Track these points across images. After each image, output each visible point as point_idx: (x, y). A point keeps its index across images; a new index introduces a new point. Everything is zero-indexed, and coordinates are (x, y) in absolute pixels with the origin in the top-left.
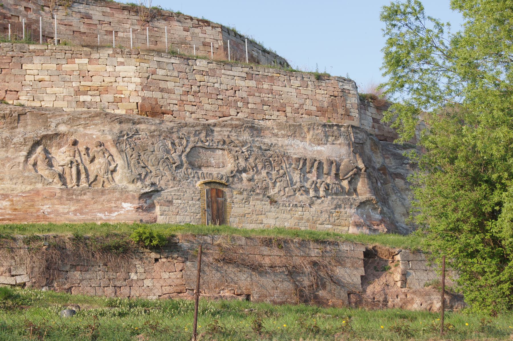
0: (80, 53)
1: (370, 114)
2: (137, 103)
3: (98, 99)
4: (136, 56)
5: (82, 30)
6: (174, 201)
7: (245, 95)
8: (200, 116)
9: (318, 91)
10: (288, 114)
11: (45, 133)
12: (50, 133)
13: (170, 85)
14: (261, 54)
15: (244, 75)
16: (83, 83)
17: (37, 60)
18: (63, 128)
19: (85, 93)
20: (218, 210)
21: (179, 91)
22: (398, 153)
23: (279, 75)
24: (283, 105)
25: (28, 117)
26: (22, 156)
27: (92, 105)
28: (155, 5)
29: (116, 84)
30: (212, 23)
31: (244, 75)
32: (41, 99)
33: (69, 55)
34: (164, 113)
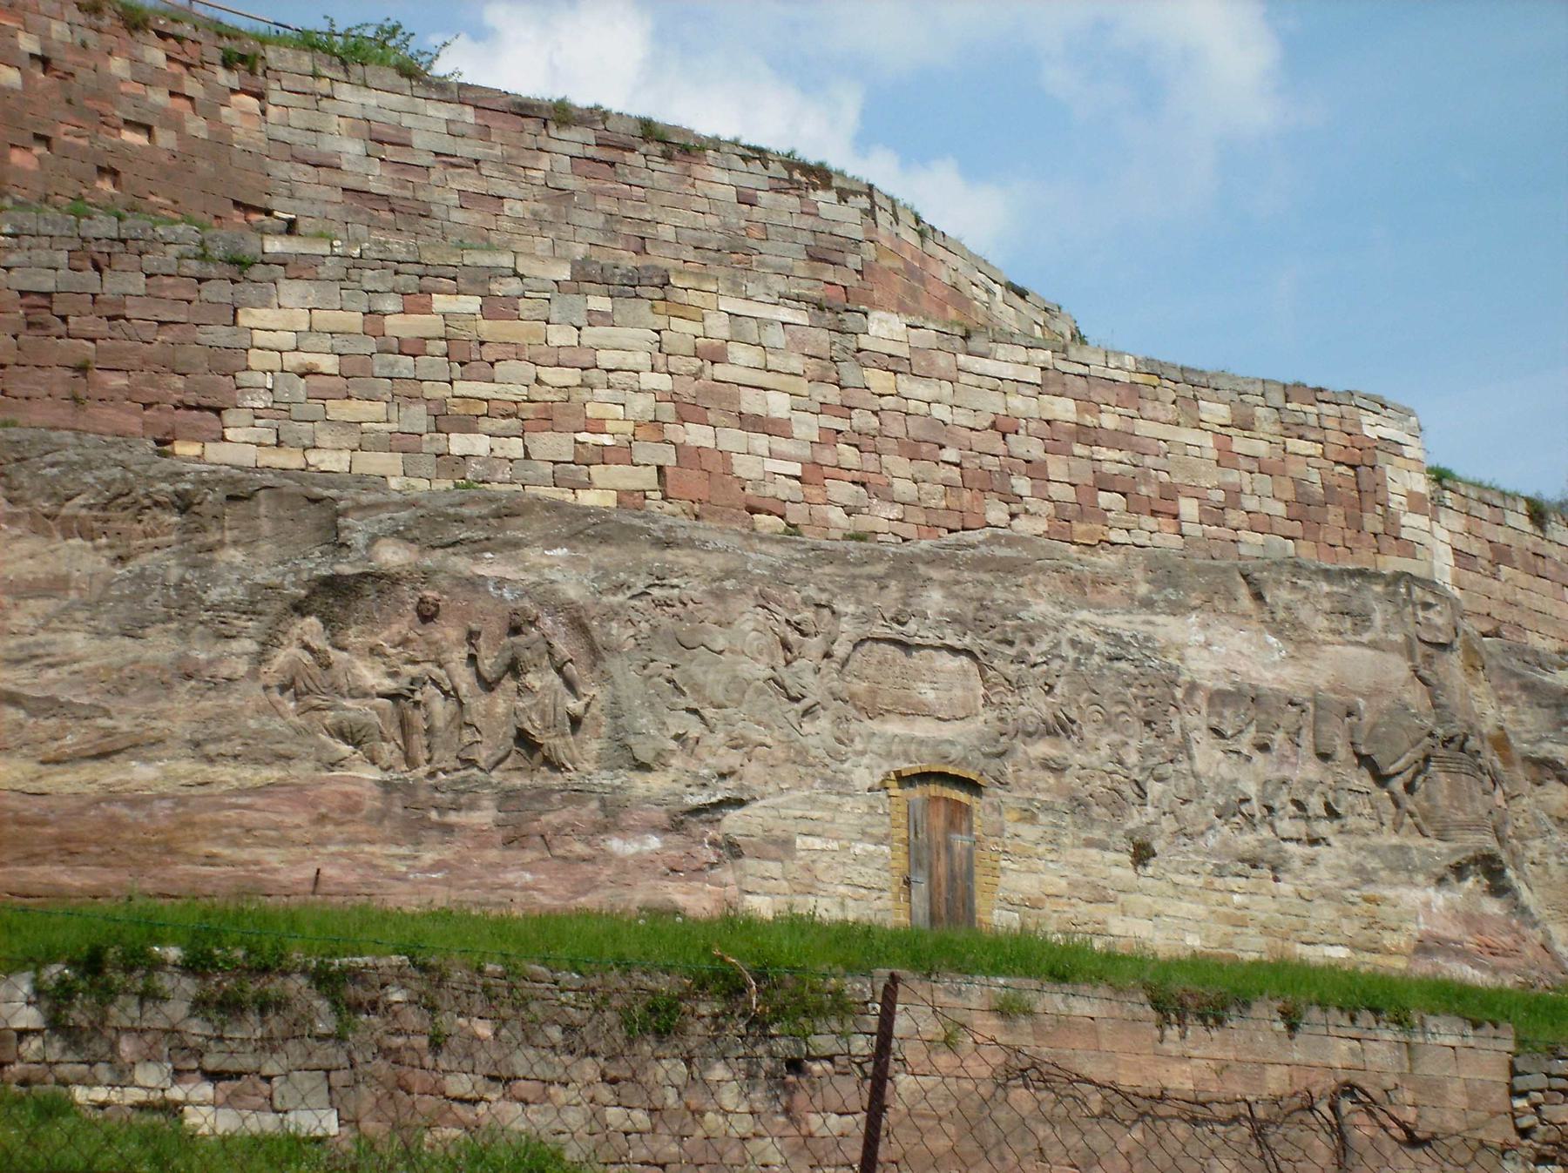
0: (451, 272)
1: (1446, 537)
2: (660, 469)
3: (515, 447)
4: (659, 294)
5: (375, 187)
6: (798, 841)
7: (1036, 450)
8: (882, 526)
9: (1294, 445)
10: (1186, 528)
11: (325, 571)
12: (345, 569)
13: (778, 405)
14: (999, 297)
15: (1035, 376)
16: (461, 387)
17: (291, 292)
18: (392, 556)
19: (467, 425)
20: (952, 877)
21: (807, 427)
22: (1543, 682)
23: (1155, 380)
24: (1170, 493)
25: (262, 510)
26: (239, 656)
27: (494, 470)
28: (556, 95)
29: (585, 394)
30: (841, 174)
31: (1035, 376)
32: (307, 443)
33: (408, 282)
34: (753, 510)
